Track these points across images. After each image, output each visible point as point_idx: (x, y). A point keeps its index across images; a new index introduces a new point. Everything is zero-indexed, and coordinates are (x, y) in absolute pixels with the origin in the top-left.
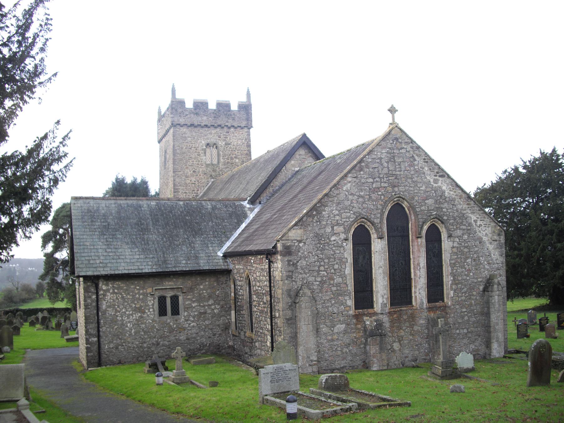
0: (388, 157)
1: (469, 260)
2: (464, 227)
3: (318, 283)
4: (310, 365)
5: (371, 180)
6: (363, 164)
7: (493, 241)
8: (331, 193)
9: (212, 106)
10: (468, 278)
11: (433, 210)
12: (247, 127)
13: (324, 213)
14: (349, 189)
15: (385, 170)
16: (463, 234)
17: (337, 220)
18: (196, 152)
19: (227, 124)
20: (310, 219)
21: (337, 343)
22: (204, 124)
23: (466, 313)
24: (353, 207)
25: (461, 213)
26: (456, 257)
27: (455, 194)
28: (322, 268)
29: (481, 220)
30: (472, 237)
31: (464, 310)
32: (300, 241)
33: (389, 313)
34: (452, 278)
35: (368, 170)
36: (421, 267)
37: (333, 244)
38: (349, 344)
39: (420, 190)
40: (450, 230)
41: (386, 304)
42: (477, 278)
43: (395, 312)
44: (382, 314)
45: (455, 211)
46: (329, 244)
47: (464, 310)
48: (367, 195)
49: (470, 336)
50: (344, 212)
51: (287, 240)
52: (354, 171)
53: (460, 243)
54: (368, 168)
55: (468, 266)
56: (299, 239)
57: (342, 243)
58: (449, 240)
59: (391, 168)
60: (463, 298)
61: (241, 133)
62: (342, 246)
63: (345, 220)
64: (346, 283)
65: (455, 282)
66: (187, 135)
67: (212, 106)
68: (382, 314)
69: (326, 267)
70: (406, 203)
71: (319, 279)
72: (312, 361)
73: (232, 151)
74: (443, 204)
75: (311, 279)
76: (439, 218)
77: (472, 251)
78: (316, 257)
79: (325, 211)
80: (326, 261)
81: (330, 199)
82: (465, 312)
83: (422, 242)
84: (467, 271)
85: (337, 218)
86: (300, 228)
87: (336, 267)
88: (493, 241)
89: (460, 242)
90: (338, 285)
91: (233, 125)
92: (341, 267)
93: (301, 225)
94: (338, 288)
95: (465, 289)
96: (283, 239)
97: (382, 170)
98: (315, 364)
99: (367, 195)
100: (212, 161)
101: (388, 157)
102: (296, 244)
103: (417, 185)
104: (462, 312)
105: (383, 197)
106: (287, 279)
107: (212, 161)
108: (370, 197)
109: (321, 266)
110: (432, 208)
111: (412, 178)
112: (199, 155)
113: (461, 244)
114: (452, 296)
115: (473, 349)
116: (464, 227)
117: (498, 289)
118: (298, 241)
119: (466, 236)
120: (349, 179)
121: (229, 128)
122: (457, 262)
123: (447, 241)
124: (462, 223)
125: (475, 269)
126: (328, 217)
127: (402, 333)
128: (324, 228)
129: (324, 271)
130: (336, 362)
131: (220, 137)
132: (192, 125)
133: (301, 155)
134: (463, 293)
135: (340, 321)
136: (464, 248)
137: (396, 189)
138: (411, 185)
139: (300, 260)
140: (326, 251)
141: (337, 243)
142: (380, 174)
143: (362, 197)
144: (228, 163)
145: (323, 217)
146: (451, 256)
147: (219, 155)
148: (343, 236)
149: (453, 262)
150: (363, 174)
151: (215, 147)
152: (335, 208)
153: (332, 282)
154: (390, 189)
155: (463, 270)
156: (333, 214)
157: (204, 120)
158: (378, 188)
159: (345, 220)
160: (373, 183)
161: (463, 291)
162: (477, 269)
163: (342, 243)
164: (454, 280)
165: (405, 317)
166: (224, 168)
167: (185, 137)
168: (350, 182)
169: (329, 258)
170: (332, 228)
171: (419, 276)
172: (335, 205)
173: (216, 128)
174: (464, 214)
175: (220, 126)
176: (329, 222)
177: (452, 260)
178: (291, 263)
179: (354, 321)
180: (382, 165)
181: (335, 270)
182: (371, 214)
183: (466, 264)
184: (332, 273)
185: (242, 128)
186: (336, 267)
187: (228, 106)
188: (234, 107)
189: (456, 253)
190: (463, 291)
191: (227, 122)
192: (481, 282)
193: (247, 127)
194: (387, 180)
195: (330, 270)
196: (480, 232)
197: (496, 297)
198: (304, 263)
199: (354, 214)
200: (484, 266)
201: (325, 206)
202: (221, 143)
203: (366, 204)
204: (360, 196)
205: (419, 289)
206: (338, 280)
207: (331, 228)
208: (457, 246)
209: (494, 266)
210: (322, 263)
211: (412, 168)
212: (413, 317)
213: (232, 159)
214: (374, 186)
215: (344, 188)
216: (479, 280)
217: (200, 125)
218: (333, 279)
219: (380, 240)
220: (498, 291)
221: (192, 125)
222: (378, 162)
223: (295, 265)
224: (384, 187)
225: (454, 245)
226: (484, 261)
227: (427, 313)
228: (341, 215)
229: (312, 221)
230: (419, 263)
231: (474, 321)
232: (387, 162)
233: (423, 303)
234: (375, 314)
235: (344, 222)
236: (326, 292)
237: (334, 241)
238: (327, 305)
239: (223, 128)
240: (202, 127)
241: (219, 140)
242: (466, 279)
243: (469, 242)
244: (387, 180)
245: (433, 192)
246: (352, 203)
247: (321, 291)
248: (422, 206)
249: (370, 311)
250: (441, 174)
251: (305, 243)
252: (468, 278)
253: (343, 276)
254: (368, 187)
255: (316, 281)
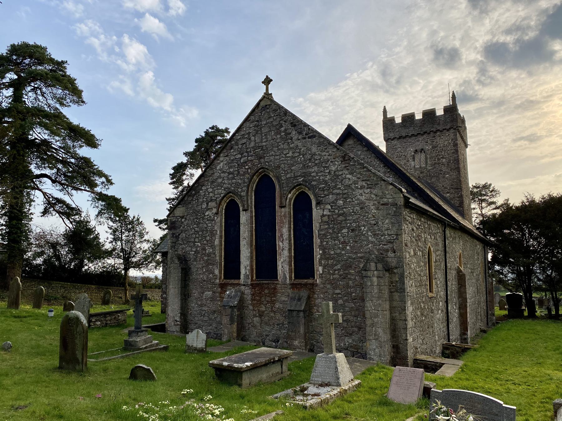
0: (255, 130)
1: (345, 231)
2: (338, 191)
3: (193, 253)
4: (175, 325)
5: (239, 156)
6: (233, 142)
7: (382, 204)
8: (207, 173)
9: (419, 116)
10: (343, 252)
11: (299, 176)
12: (452, 128)
13: (201, 192)
14: (222, 167)
15: (252, 144)
16: (336, 200)
17: (211, 197)
18: (405, 159)
19: (432, 129)
20: (190, 199)
21: (205, 309)
22: (411, 134)
23: (340, 296)
24: (224, 183)
25: (335, 175)
26: (326, 227)
27: (327, 154)
28: (197, 240)
29: (363, 181)
30: (350, 202)
31: (338, 291)
32: (182, 217)
33: (252, 285)
34: (321, 252)
35: (237, 147)
36: (284, 238)
37: (207, 219)
38: (215, 312)
39: (286, 157)
40: (319, 197)
41: (248, 276)
42: (356, 253)
43: (258, 285)
44: (244, 285)
45: (327, 174)
46: (203, 218)
47: (338, 291)
48: (235, 171)
49: (346, 326)
50: (217, 189)
51: (173, 217)
52: (225, 151)
53: (332, 210)
54: (237, 145)
55: (343, 237)
56: (181, 215)
57: (214, 217)
58: (319, 208)
59: (258, 140)
60: (336, 276)
61: (447, 134)
62: (213, 220)
63: (217, 196)
64: (214, 254)
65: (325, 256)
66: (397, 147)
67: (419, 116)
68: (244, 285)
69: (200, 238)
70: (271, 173)
71: (194, 250)
72: (176, 320)
73: (439, 152)
74: (310, 168)
75: (188, 249)
76: (307, 183)
77: (349, 220)
78: (193, 230)
79: (202, 190)
80: (200, 233)
81: (206, 179)
82: (339, 294)
83: (285, 212)
84: (342, 243)
85: (211, 195)
86: (183, 206)
87: (208, 238)
88: (382, 204)
89: (332, 208)
90: (209, 255)
91: (438, 129)
92: (212, 239)
93: (184, 204)
94: (209, 258)
95: (339, 267)
96: (170, 216)
97: (250, 144)
98: (178, 325)
99: (235, 171)
100: (420, 164)
101: (255, 130)
102: (180, 220)
103: (282, 153)
104: (334, 293)
105: (249, 170)
106: (171, 249)
107: (420, 164)
108: (239, 172)
109: (196, 237)
110: (299, 174)
111: (278, 147)
112: (408, 161)
113: (334, 212)
114: (321, 272)
115: (350, 343)
116: (338, 191)
117: (376, 268)
118: (180, 217)
119: (341, 202)
120: (221, 159)
121: (435, 132)
122: (327, 232)
123: (315, 209)
124: (335, 186)
125: (353, 241)
126: (204, 195)
127: (263, 308)
128: (201, 204)
129: (198, 242)
130: (204, 327)
131: (427, 142)
132: (400, 137)
133: (349, 145)
134: (335, 270)
135: (208, 288)
136: (339, 216)
137: (262, 160)
138: (277, 154)
139: (181, 233)
140: (201, 225)
141: (210, 217)
142: (247, 149)
143: (232, 173)
144: (435, 164)
145: (200, 195)
146: (320, 226)
147: (426, 159)
148: (215, 211)
149: (323, 233)
150: (233, 152)
151: (423, 152)
152: (209, 187)
153: (204, 252)
154: (256, 162)
155: (336, 242)
156: (208, 192)
157: (411, 131)
158: (246, 162)
159: (217, 196)
160: (241, 158)
161: (336, 268)
162: (356, 242)
163: (214, 217)
164: (324, 252)
165: (266, 291)
166: (431, 169)
167: (396, 148)
168: (222, 161)
169: (203, 231)
170: (207, 204)
171: (281, 248)
172: (209, 184)
173: (422, 135)
174: (338, 176)
175: (425, 133)
176: (204, 199)
177: (322, 230)
178: (175, 236)
179: (219, 289)
180: (250, 139)
181: (207, 241)
182: (238, 188)
183: (340, 235)
184: (205, 244)
185: (448, 130)
186: (208, 238)
187: (412, 116)
188: (440, 112)
189: (327, 222)
190: (336, 268)
191: (433, 127)
192: (361, 258)
193: (452, 128)
194: (254, 153)
195: (203, 241)
196: (362, 195)
197: (375, 279)
198: (184, 235)
199: (224, 190)
200: (368, 238)
201: (202, 186)
202: (428, 147)
203: (236, 179)
204: (230, 173)
205: (282, 263)
206: (209, 250)
207: (206, 205)
208: (329, 213)
209: (382, 238)
210: (197, 236)
211: (278, 136)
212: (274, 292)
213: (439, 159)
214: (242, 161)
215: (218, 168)
216: (359, 255)
217: (408, 135)
218: (205, 250)
219: (245, 212)
220: (376, 270)
221: (400, 137)
222: (246, 138)
223: (177, 237)
224: (251, 161)
225: (325, 213)
226: (367, 231)
227: (290, 289)
228: (214, 192)
229: (192, 200)
230: (282, 235)
231: (352, 307)
232: (254, 136)
233: (286, 278)
234: (239, 284)
235: (217, 198)
236: (200, 261)
237: (208, 215)
238: (200, 272)
239: (429, 134)
240: (410, 137)
241: (426, 145)
242: (340, 253)
243: (345, 208)
244: (254, 153)
245: (301, 156)
246: (223, 180)
247: (195, 260)
248: (288, 173)
249: (236, 281)
250: (311, 134)
251: (186, 219)
252: (343, 252)
253: (213, 247)
254: (237, 163)
255: (192, 251)
